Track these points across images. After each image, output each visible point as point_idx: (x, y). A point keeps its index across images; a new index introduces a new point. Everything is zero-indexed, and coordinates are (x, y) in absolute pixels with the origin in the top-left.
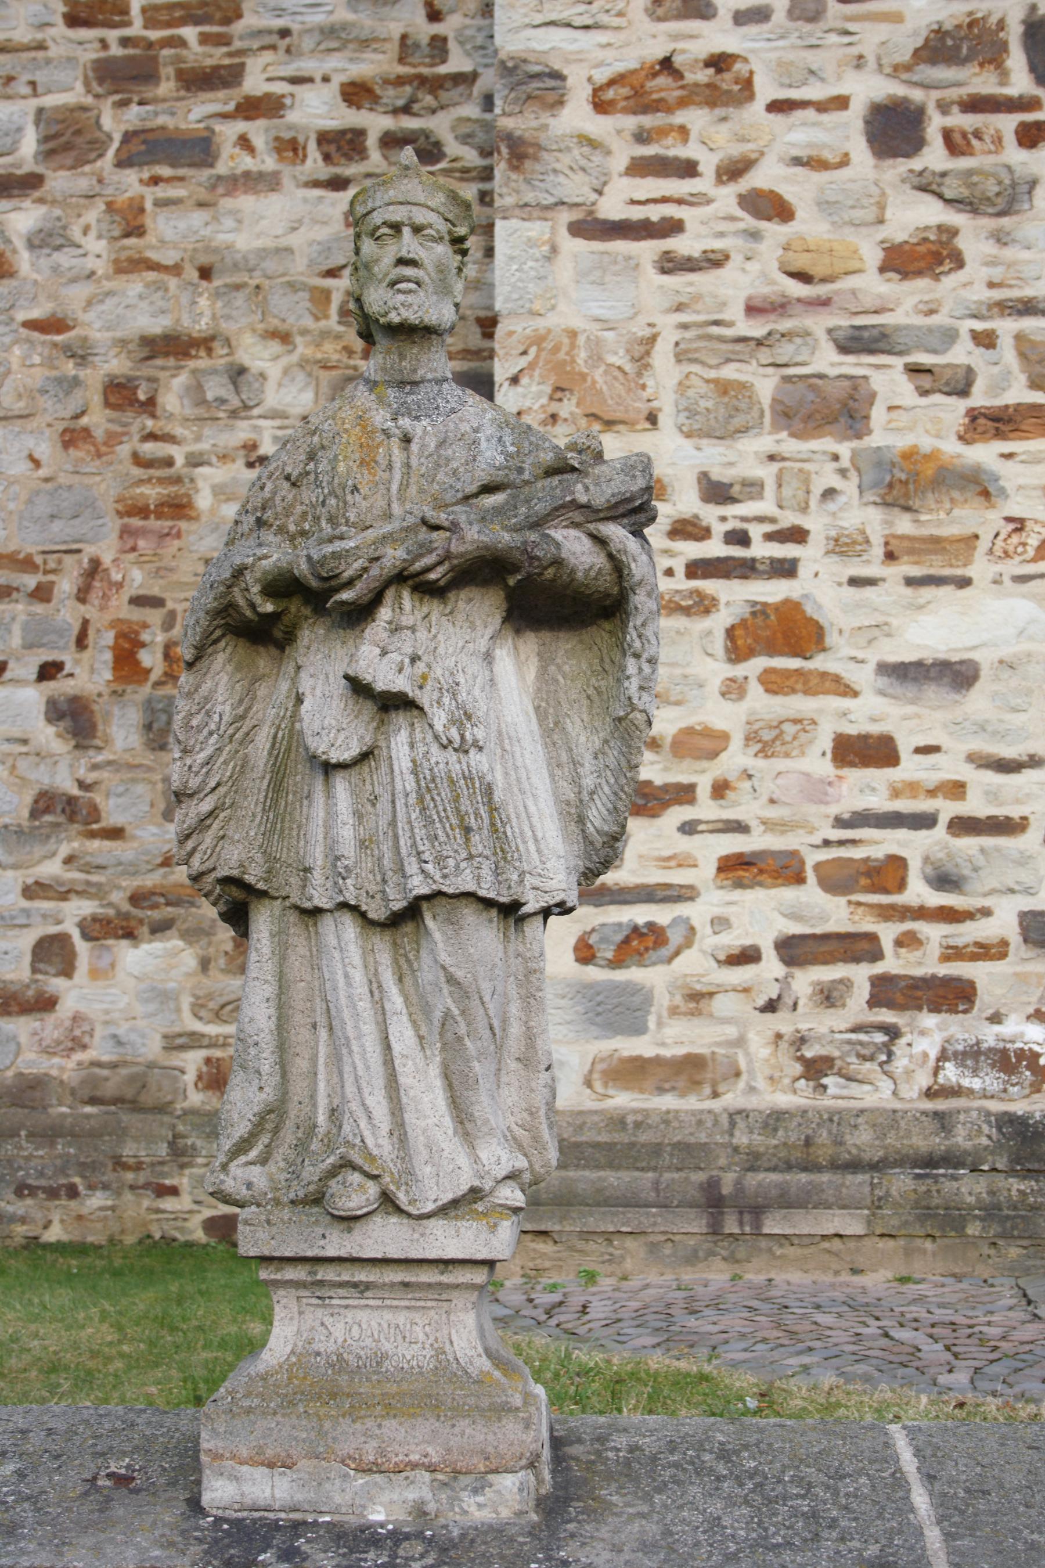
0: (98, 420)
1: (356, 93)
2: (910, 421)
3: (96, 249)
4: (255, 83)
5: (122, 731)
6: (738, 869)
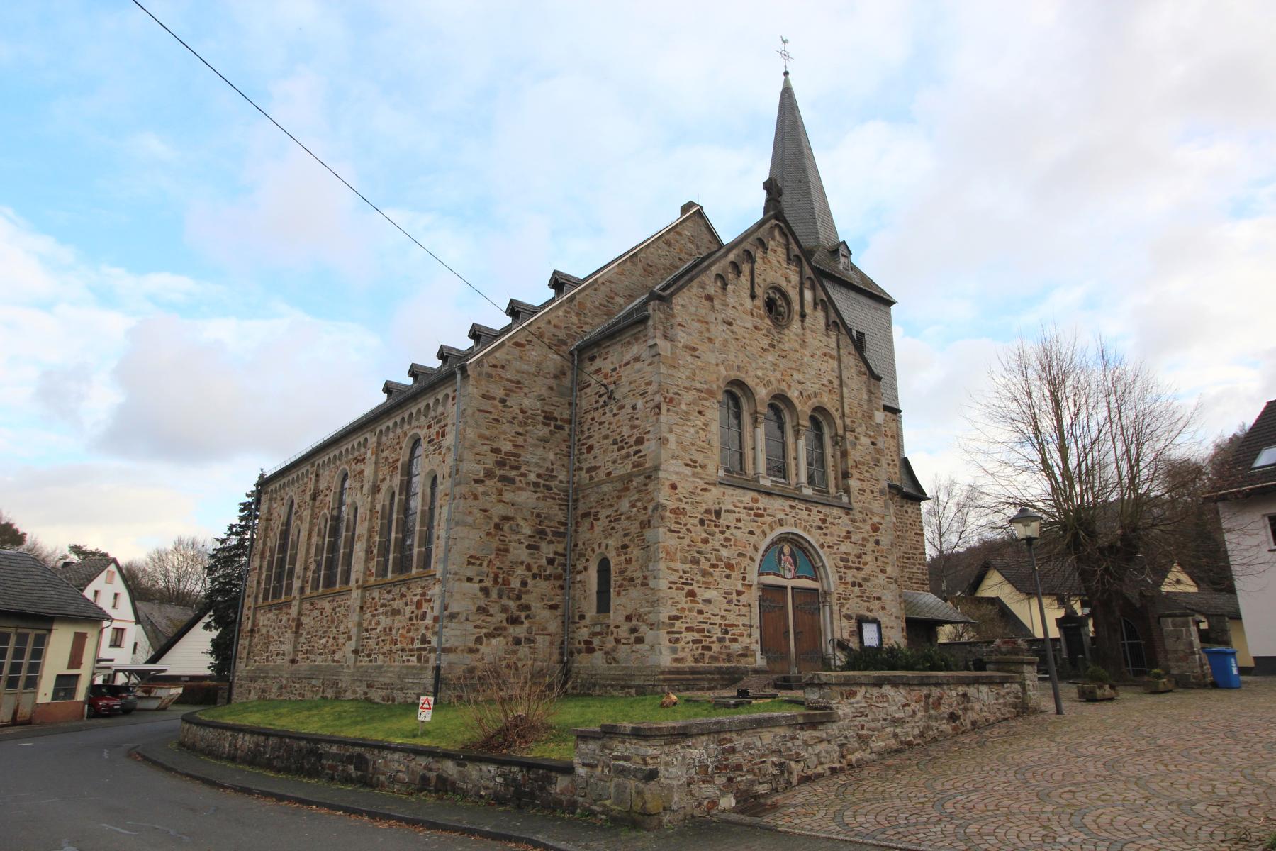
0: (492, 531)
1: (539, 476)
2: (705, 565)
3: (494, 497)
4: (523, 470)
5: (494, 595)
6: (689, 629)
